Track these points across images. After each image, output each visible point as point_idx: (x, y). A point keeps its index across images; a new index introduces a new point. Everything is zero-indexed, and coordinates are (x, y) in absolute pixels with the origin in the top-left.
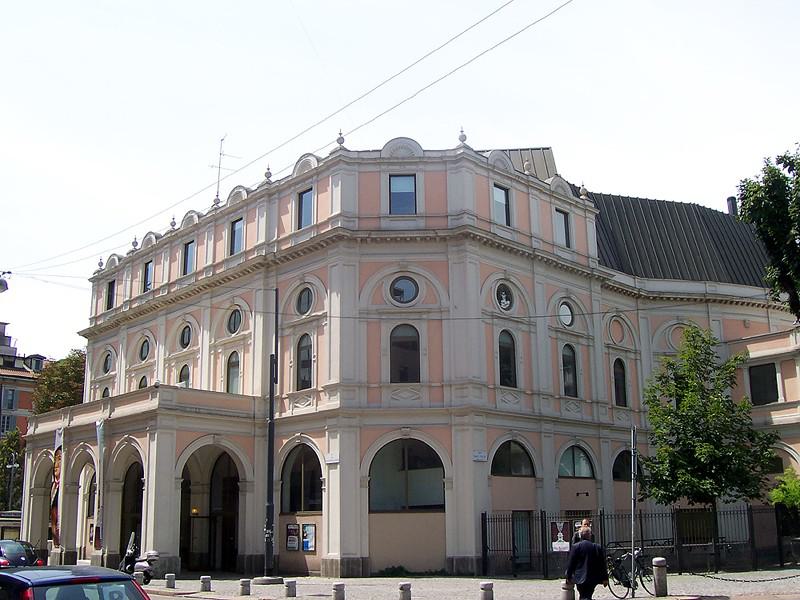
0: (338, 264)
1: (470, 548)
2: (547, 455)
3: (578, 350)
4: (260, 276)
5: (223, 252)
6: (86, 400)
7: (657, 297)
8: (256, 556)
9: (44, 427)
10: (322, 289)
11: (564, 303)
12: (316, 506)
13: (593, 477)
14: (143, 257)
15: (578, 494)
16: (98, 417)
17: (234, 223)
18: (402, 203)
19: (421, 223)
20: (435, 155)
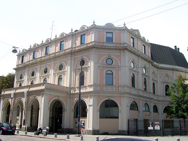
0: (93, 54)
1: (125, 128)
3: (147, 80)
5: (31, 58)
6: (15, 87)
7: (162, 68)
9: (7, 93)
10: (88, 60)
12: (85, 115)
13: (149, 111)
15: (146, 115)
16: (25, 90)
17: (61, 42)
18: (109, 40)
19: (114, 45)
20: (117, 28)
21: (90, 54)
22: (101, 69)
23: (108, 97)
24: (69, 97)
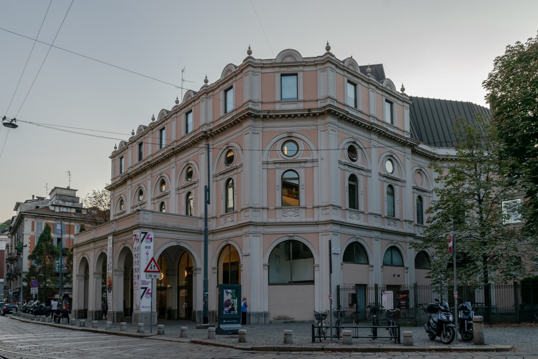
2: (376, 250)
11: (389, 159)
13: (403, 266)
14: (139, 139)
22: (269, 168)
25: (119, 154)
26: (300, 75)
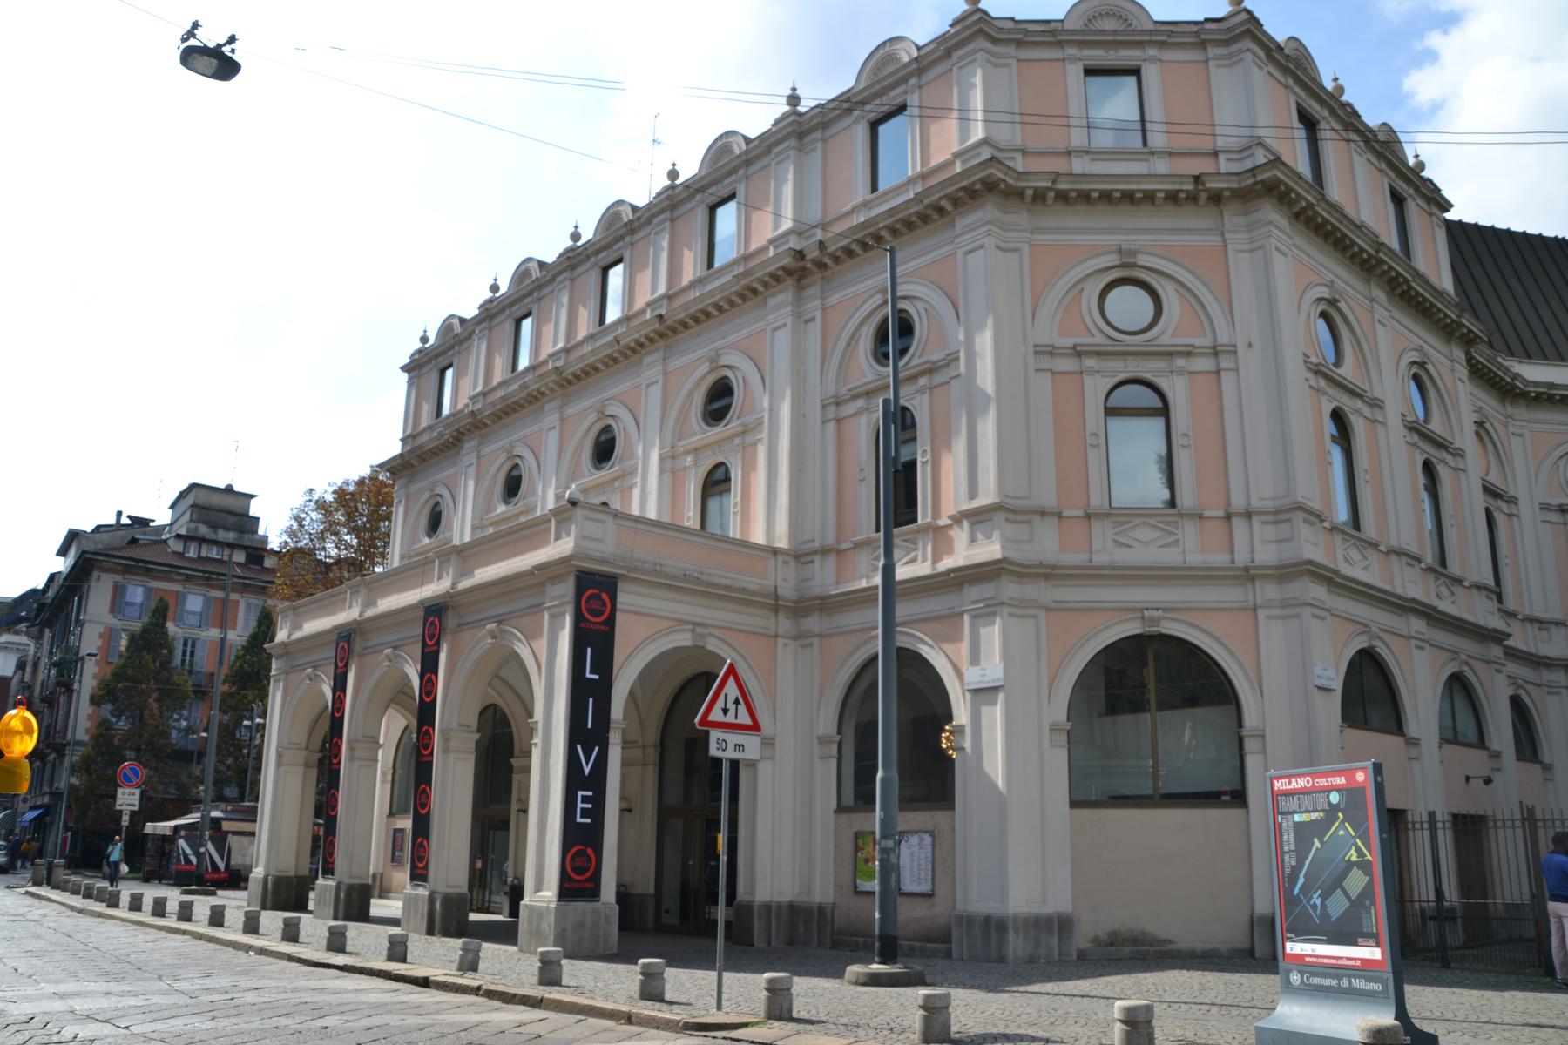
4: (783, 297)
8: (779, 905)
21: (960, 252)
22: (1056, 369)
23: (1141, 610)
24: (795, 638)
25: (437, 356)
26: (1151, 73)
